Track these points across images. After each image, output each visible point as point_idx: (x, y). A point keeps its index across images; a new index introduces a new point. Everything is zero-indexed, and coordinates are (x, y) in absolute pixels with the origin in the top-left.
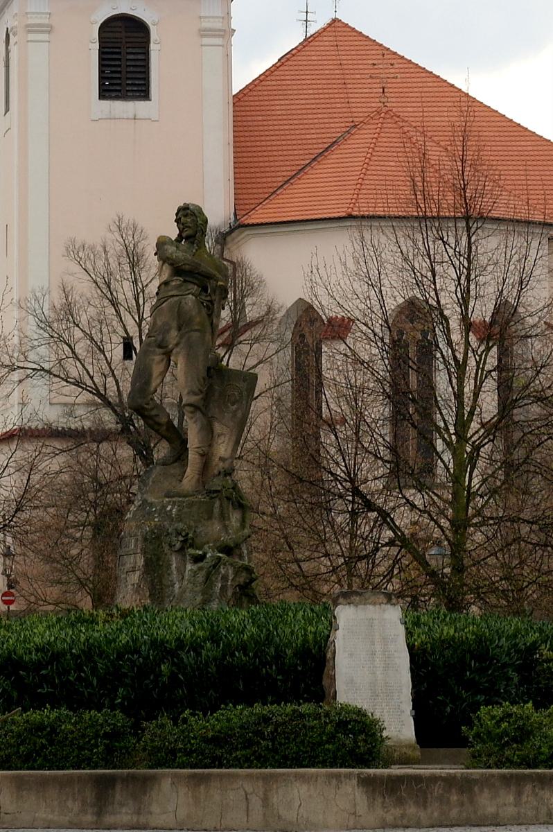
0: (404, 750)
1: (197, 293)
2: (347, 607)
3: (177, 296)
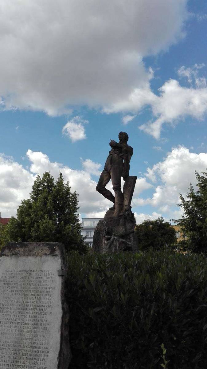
1: (118, 153)
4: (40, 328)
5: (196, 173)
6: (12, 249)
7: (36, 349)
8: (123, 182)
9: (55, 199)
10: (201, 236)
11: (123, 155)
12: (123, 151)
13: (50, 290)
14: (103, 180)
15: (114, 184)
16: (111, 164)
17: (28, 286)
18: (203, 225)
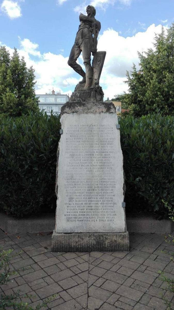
0: (114, 238)
1: (88, 27)
2: (71, 115)
3: (82, 28)
4: (107, 168)
5: (139, 53)
6: (72, 108)
7: (105, 183)
8: (92, 57)
9: (13, 72)
10: (140, 107)
11: (93, 30)
12: (93, 26)
13: (112, 140)
14: (74, 54)
15: (85, 58)
16: (82, 38)
17: (92, 137)
18: (143, 99)
